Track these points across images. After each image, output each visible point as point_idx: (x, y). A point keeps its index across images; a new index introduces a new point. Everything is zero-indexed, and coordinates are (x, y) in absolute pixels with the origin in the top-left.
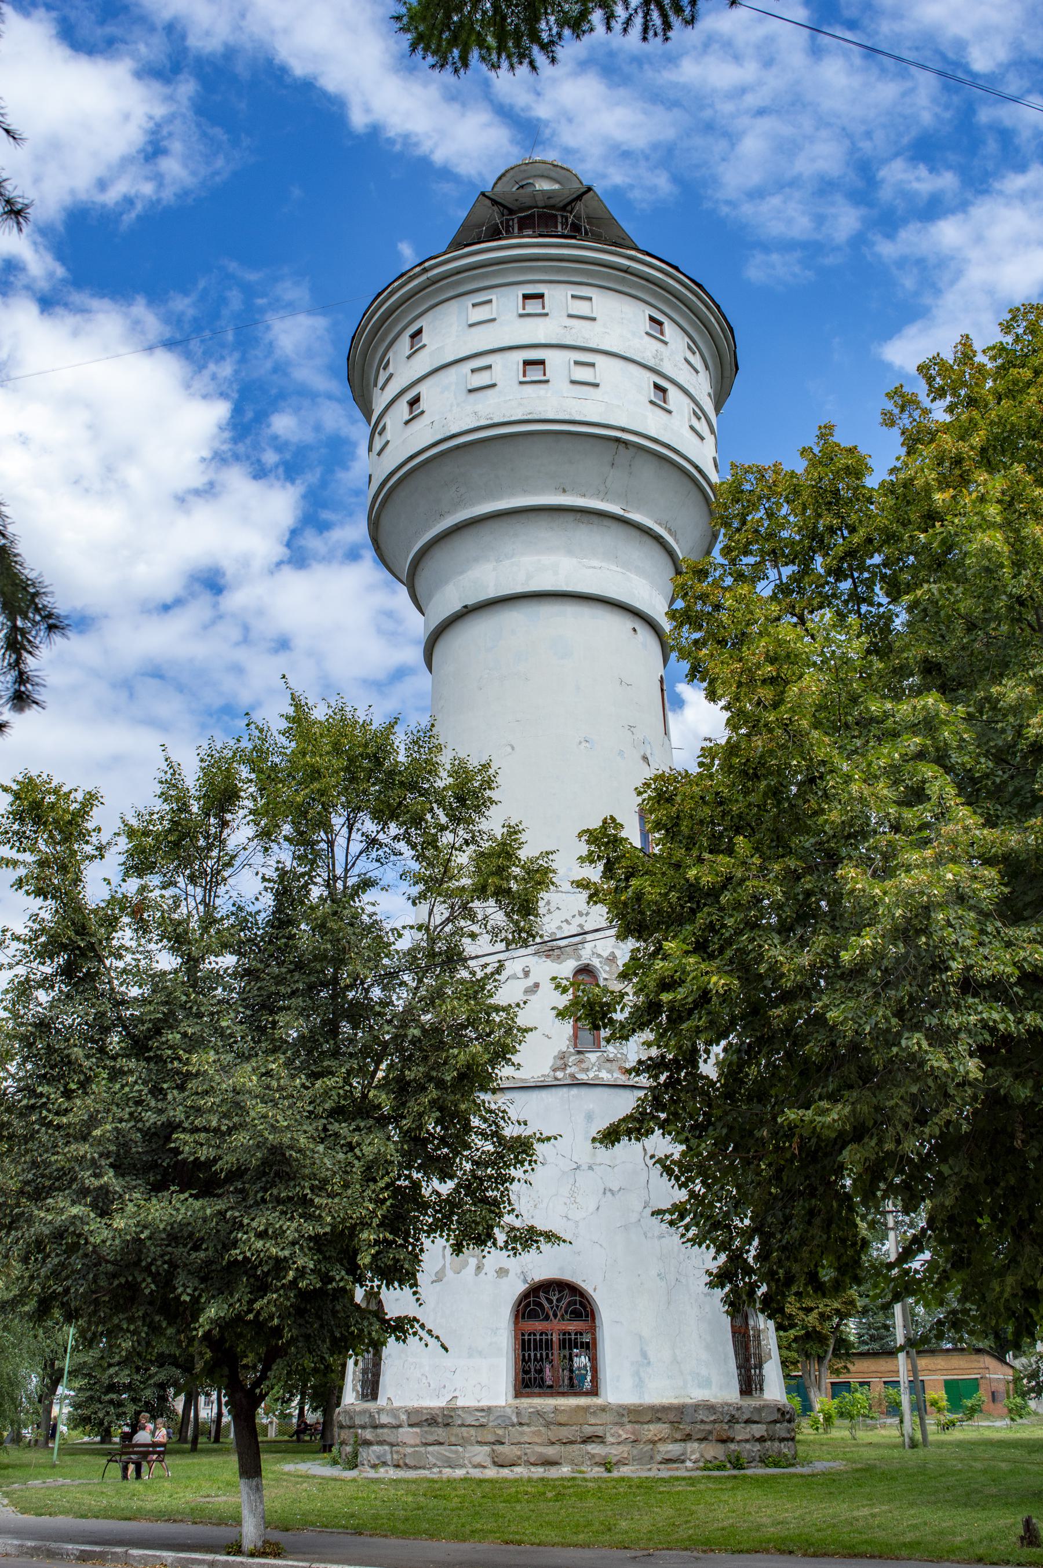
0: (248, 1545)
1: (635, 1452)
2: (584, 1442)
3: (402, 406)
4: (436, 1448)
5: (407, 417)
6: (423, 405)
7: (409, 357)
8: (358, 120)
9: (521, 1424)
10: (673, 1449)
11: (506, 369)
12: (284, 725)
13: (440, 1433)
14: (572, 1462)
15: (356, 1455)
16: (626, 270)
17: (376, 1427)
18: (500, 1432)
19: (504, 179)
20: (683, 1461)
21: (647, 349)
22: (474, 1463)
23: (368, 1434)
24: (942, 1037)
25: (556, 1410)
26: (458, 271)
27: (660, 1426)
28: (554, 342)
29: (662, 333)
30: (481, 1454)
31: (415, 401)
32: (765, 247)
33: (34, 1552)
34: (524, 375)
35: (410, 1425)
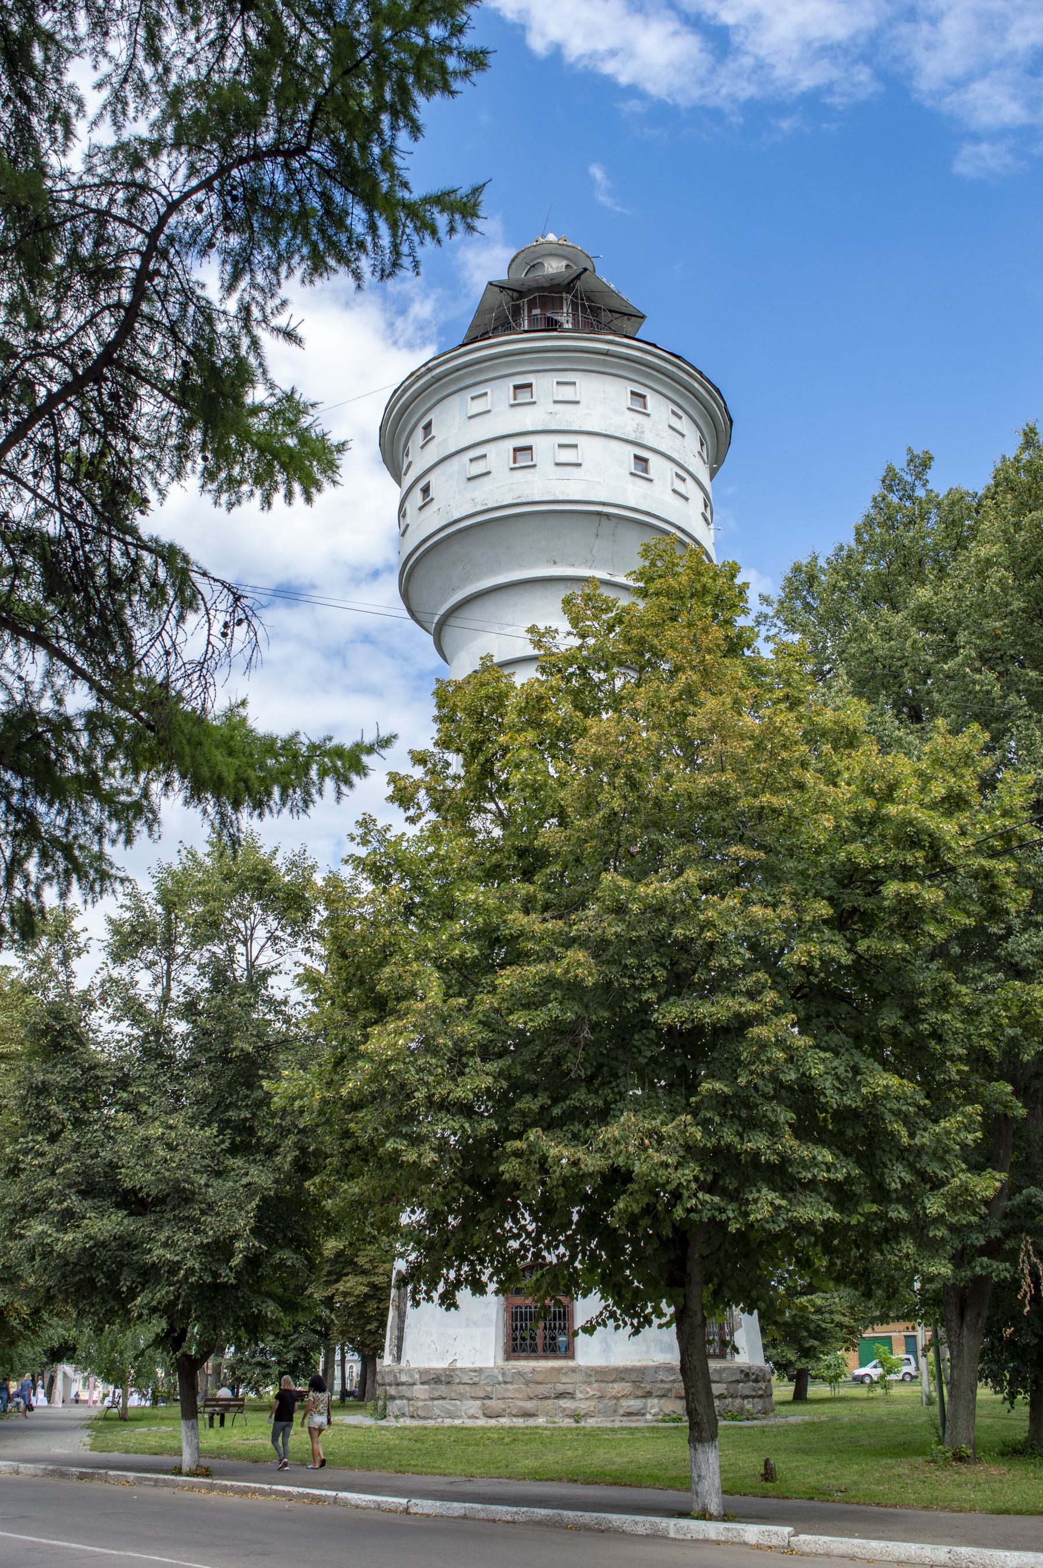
0: (185, 1468)
1: (601, 1406)
2: (557, 1397)
3: (417, 493)
4: (440, 1402)
5: (421, 504)
6: (433, 493)
7: (422, 447)
8: (538, 44)
9: (505, 1383)
10: (635, 1404)
11: (500, 455)
12: (208, 849)
13: (443, 1390)
14: (547, 1414)
15: (385, 1407)
16: (607, 353)
17: (398, 1384)
18: (489, 1389)
19: (517, 261)
20: (643, 1415)
21: (628, 424)
22: (468, 1415)
23: (392, 1391)
24: (415, 1141)
25: (534, 1371)
26: (458, 369)
27: (623, 1385)
28: (540, 428)
29: (645, 407)
30: (474, 1406)
31: (426, 490)
32: (976, 138)
33: (52, 1473)
34: (515, 462)
35: (422, 1383)
